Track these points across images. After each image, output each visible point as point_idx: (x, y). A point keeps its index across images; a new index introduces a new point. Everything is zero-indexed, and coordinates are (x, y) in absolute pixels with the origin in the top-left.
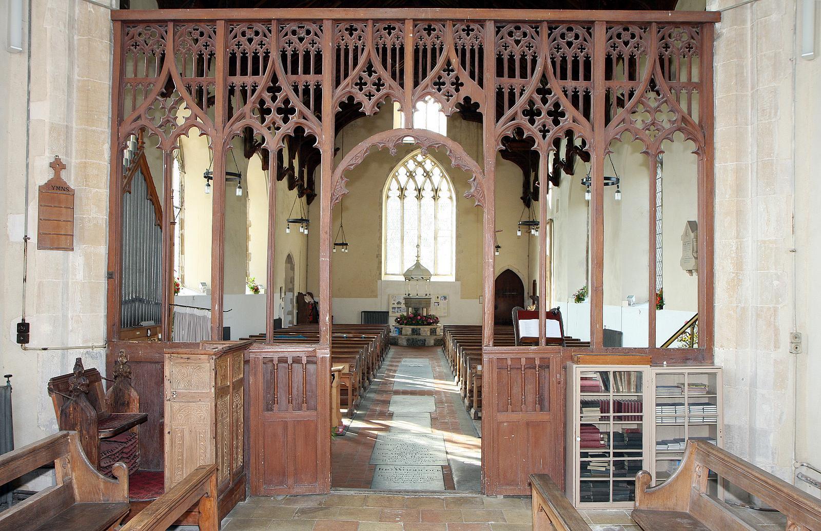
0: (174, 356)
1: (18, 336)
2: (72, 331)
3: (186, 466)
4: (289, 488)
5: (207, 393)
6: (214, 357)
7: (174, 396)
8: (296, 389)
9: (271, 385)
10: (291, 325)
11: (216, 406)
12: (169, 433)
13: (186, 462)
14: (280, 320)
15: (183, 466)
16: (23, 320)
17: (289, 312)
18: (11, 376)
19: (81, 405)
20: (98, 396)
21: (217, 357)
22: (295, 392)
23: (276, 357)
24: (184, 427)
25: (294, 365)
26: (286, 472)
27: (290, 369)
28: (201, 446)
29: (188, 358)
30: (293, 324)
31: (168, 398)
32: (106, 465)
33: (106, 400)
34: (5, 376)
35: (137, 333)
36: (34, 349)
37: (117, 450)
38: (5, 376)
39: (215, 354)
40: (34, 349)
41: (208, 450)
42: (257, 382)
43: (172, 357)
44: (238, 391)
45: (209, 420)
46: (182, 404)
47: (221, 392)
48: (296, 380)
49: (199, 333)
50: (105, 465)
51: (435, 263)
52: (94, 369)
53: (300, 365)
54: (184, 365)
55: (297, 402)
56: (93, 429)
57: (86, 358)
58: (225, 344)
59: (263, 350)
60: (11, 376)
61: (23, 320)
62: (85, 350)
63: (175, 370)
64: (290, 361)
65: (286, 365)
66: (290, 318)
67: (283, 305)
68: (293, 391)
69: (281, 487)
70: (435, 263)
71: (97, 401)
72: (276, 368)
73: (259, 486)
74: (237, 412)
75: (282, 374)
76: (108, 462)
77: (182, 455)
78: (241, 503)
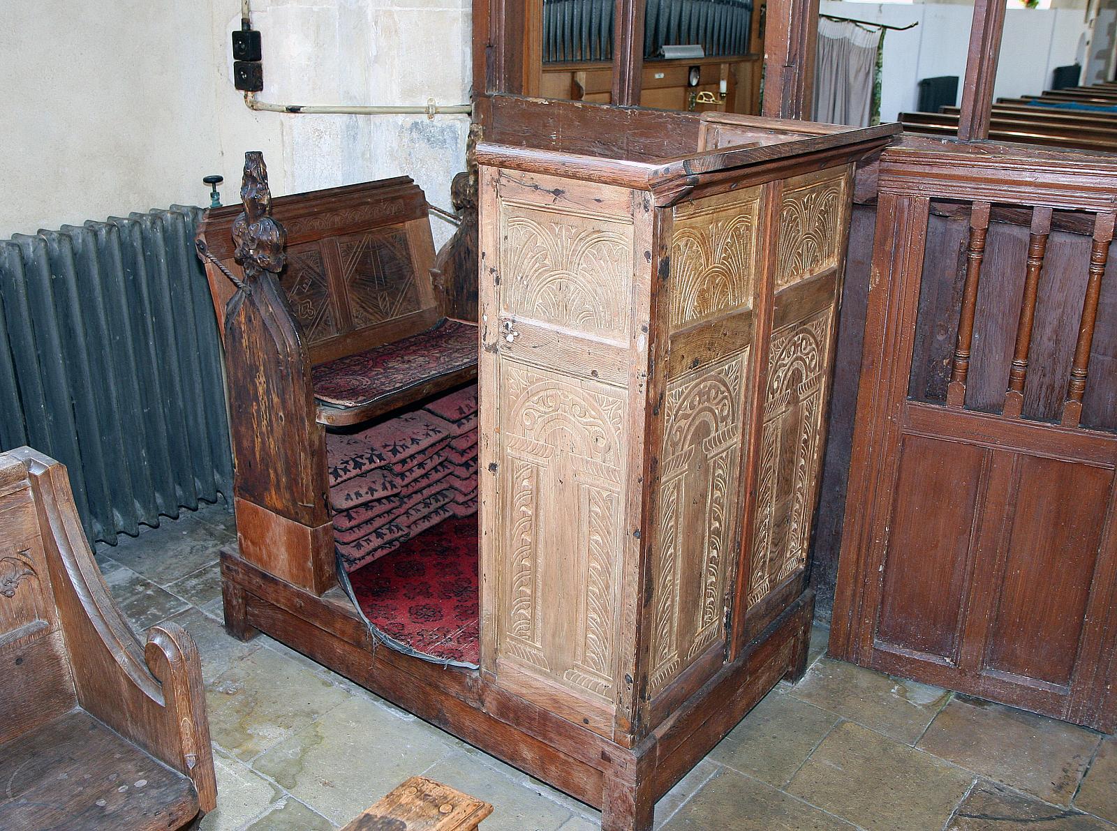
0: (509, 178)
1: (238, 69)
2: (377, 59)
3: (544, 601)
4: (962, 672)
5: (620, 351)
6: (653, 200)
7: (510, 338)
8: (1048, 331)
9: (950, 299)
10: (1100, 82)
11: (654, 409)
12: (493, 467)
13: (545, 584)
14: (1076, 69)
15: (534, 591)
16: (246, 22)
17: (1100, 52)
18: (220, 179)
19: (263, 312)
20: (410, 262)
21: (662, 201)
22: (1044, 340)
23: (982, 199)
24: (541, 461)
25: (1059, 238)
26: (960, 618)
27: (1041, 248)
28: (593, 546)
29: (557, 192)
30: (1105, 78)
31: (490, 340)
32: (350, 504)
33: (435, 276)
34: (207, 181)
35: (657, 76)
36: (272, 109)
37: (413, 449)
38: (207, 181)
39: (654, 187)
40: (272, 109)
41: (617, 570)
42: (896, 294)
43: (503, 181)
44: (803, 323)
45: (624, 461)
46: (536, 374)
47: (669, 349)
48: (1058, 297)
49: (827, 88)
50: (345, 505)
51: (429, 411)
52: (405, 181)
53: (1083, 243)
54: (545, 217)
55: (1047, 380)
56: (297, 396)
57: (412, 140)
58: (784, 132)
59: (935, 170)
60: (220, 179)
61: (246, 22)
62: (410, 119)
63: (517, 236)
64: (1040, 221)
65: (1021, 233)
66: (1100, 65)
67: (1089, 37)
68: (1037, 336)
69: (934, 659)
70: (429, 411)
71: (402, 277)
72: (977, 243)
73: (857, 635)
74: (794, 401)
75: (1004, 268)
76: (363, 491)
77: (534, 557)
78: (784, 688)
